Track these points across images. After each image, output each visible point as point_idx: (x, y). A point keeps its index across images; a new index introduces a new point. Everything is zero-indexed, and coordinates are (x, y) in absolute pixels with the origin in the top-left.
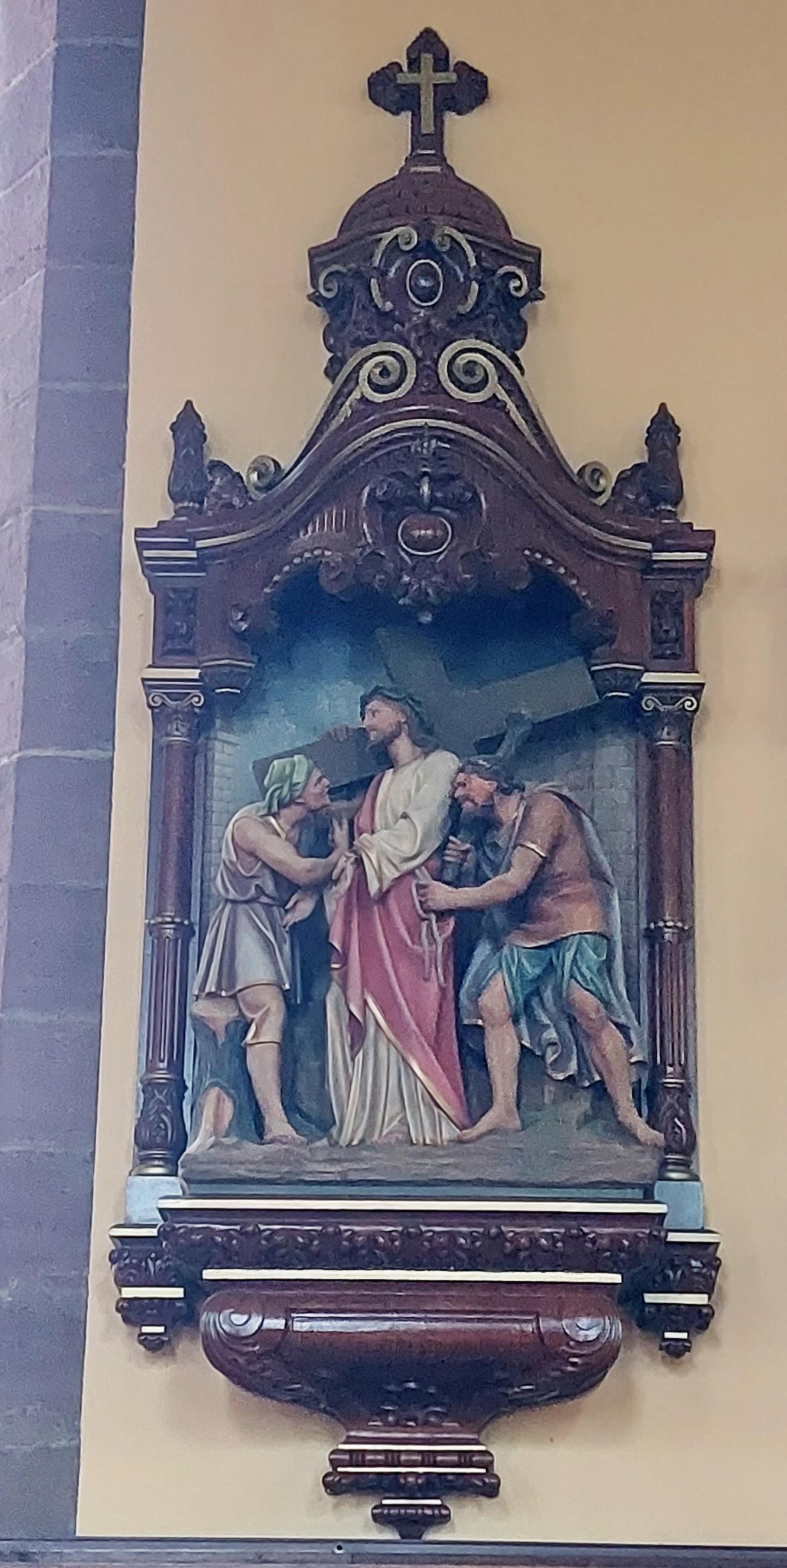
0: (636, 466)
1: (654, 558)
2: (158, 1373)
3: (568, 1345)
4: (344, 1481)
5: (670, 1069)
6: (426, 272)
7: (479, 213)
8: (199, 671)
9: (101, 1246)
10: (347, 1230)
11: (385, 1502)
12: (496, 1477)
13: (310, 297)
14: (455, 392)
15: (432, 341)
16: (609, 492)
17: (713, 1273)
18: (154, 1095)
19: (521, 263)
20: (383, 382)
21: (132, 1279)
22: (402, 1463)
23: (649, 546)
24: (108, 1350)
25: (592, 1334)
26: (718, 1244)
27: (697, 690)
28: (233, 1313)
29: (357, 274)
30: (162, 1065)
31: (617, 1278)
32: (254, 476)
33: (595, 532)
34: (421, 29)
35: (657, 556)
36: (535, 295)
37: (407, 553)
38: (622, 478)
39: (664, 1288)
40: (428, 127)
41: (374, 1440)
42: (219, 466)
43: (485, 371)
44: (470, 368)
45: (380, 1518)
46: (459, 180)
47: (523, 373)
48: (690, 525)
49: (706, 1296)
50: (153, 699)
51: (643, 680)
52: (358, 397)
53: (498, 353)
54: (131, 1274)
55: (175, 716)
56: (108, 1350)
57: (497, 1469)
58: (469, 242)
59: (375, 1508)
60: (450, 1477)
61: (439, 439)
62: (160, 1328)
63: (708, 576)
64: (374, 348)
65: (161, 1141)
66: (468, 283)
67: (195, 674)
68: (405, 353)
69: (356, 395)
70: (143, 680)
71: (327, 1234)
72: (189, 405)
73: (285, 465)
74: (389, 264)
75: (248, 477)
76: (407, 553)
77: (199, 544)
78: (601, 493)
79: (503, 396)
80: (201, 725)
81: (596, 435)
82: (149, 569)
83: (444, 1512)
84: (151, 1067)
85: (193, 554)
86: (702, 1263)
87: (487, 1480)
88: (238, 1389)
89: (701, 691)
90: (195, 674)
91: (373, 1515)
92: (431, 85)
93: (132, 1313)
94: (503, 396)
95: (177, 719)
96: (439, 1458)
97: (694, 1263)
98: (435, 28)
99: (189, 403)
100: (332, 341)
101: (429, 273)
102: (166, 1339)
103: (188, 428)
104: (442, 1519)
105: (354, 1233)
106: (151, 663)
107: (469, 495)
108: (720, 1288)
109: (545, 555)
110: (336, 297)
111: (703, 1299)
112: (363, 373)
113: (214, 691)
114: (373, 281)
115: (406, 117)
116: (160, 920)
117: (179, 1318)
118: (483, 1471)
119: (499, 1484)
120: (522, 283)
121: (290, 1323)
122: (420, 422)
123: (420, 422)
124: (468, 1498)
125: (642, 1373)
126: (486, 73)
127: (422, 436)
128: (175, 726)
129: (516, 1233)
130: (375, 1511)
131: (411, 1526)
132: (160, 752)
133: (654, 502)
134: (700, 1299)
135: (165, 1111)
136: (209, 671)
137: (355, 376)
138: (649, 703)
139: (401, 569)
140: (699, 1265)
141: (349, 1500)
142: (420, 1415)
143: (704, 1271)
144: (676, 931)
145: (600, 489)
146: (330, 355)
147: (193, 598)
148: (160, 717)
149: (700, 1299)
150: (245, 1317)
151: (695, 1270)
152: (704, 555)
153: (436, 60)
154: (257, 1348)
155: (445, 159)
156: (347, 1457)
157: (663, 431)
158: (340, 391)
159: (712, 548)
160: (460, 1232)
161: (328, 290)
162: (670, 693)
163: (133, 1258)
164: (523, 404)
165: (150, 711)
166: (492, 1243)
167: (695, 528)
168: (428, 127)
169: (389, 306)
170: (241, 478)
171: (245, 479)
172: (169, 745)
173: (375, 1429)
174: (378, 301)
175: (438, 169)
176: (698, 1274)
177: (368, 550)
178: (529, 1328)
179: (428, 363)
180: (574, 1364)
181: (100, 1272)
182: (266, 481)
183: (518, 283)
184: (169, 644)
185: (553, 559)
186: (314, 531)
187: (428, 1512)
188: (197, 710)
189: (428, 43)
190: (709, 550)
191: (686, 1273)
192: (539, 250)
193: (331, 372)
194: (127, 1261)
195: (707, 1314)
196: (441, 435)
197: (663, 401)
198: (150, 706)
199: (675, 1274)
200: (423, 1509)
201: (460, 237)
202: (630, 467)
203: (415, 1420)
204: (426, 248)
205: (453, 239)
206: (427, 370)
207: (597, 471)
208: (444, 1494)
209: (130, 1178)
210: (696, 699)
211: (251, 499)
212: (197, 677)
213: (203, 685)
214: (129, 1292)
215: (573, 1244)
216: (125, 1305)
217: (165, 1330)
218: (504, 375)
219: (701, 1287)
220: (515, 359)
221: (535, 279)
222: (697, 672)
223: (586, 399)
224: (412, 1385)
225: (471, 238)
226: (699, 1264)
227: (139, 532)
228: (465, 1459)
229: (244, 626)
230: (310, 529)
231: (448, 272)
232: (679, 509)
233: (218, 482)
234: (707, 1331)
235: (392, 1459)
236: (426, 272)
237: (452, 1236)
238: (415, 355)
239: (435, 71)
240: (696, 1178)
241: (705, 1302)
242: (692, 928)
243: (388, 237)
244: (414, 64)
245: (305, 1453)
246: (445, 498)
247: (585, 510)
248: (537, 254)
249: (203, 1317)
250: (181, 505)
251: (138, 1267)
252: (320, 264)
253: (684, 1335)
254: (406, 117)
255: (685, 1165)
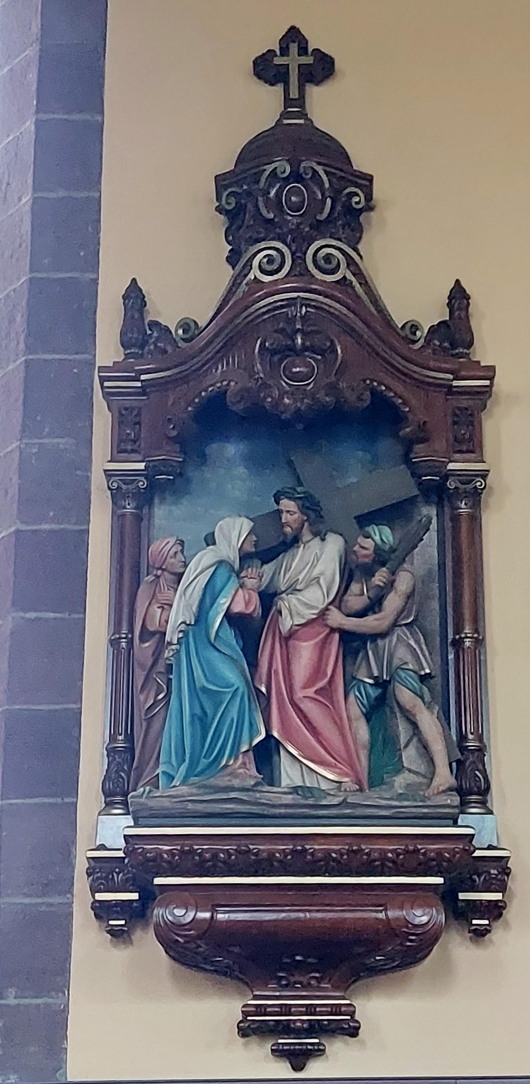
0: (440, 322)
1: (454, 385)
2: (121, 955)
3: (407, 927)
4: (252, 1026)
5: (471, 737)
6: (293, 191)
7: (332, 152)
8: (144, 464)
9: (81, 865)
10: (310, 849)
11: (280, 1041)
12: (358, 1022)
13: (217, 209)
14: (319, 275)
15: (298, 243)
16: (422, 340)
17: (506, 878)
18: (115, 759)
19: (357, 185)
20: (269, 268)
21: (102, 887)
22: (344, 1013)
23: (451, 377)
24: (87, 938)
25: (425, 919)
26: (509, 857)
27: (484, 475)
28: (174, 908)
29: (249, 193)
30: (120, 738)
31: (440, 880)
32: (180, 332)
33: (415, 368)
34: (289, 27)
35: (455, 383)
36: (369, 208)
37: (286, 383)
38: (432, 330)
39: (470, 890)
40: (294, 94)
41: (272, 998)
42: (155, 324)
43: (338, 260)
44: (328, 258)
45: (279, 1052)
46: (317, 129)
47: (361, 257)
48: (479, 362)
49: (501, 894)
50: (112, 484)
51: (448, 468)
52: (253, 278)
53: (344, 247)
54: (101, 884)
55: (127, 495)
56: (87, 938)
57: (357, 1017)
58: (325, 171)
59: (272, 1046)
60: (326, 1022)
61: (307, 306)
62: (122, 922)
63: (490, 396)
64: (263, 245)
65: (116, 794)
66: (324, 199)
67: (142, 466)
68: (285, 249)
69: (251, 276)
70: (105, 471)
71: (353, 851)
72: (134, 281)
73: (202, 324)
74: (271, 186)
75: (176, 331)
76: (286, 383)
77: (143, 377)
78: (417, 341)
79: (350, 276)
80: (146, 498)
81: (413, 301)
82: (107, 395)
83: (321, 1047)
84: (113, 738)
85: (139, 384)
86: (498, 871)
87: (351, 1024)
88: (177, 965)
89: (487, 475)
90: (142, 466)
91: (272, 1050)
92: (295, 65)
93: (102, 911)
94: (350, 276)
95: (128, 497)
96: (269, 1010)
97: (492, 871)
98: (297, 26)
99: (134, 280)
100: (231, 238)
101: (299, 193)
102: (126, 929)
103: (134, 297)
104: (318, 1052)
105: (259, 850)
106: (109, 459)
107: (328, 344)
108: (510, 888)
109: (380, 384)
110: (234, 208)
111: (499, 896)
112: (256, 262)
113: (154, 477)
114: (260, 199)
115: (279, 88)
116: (118, 636)
117: (137, 914)
118: (349, 1017)
119: (359, 1028)
120: (360, 199)
121: (215, 914)
122: (294, 295)
123: (294, 295)
124: (337, 1040)
125: (457, 947)
126: (333, 56)
127: (295, 305)
128: (127, 502)
129: (315, 850)
130: (273, 1048)
131: (298, 1058)
132: (118, 519)
133: (454, 346)
134: (497, 896)
135: (123, 771)
136: (151, 464)
137: (249, 264)
138: (451, 484)
139: (283, 394)
140: (497, 872)
141: (254, 1039)
142: (304, 980)
143: (499, 876)
144: (474, 640)
145: (416, 339)
146: (230, 247)
147: (139, 414)
148: (117, 496)
149: (497, 896)
150: (184, 911)
151: (493, 876)
152: (487, 383)
153: (300, 48)
154: (192, 932)
155: (306, 115)
156: (304, 1009)
157: (458, 297)
158: (239, 274)
159: (493, 377)
160: (331, 849)
161: (229, 204)
162: (467, 478)
163: (104, 872)
164: (364, 283)
165: (109, 492)
166: (356, 858)
167: (482, 364)
168: (294, 94)
169: (271, 216)
170: (171, 332)
171: (173, 332)
172: (124, 515)
173: (274, 990)
174: (264, 212)
175: (302, 121)
176: (494, 878)
177: (260, 382)
178: (382, 916)
179: (299, 254)
180: (411, 941)
181: (81, 883)
182: (190, 334)
183: (357, 199)
184: (120, 449)
185: (385, 386)
186: (223, 367)
187: (309, 1047)
188: (142, 491)
189: (293, 36)
190: (491, 379)
191: (487, 878)
192: (372, 176)
193: (233, 259)
194: (99, 875)
195: (502, 907)
196: (306, 303)
197: (457, 278)
198: (109, 488)
199: (479, 879)
200: (283, 1047)
201: (320, 169)
202: (436, 323)
203: (300, 983)
204: (296, 176)
205: (315, 172)
206: (299, 258)
207: (415, 327)
208: (320, 1035)
209: (100, 817)
210: (485, 481)
211: (179, 347)
212: (143, 468)
213: (149, 474)
214: (100, 896)
215: (411, 858)
216: (97, 905)
217: (126, 922)
218: (351, 262)
219: (497, 888)
220: (356, 250)
221: (369, 197)
222: (484, 462)
223: (406, 276)
224: (298, 958)
225: (328, 169)
226: (496, 872)
227: (99, 367)
228: (336, 1010)
229: (175, 433)
230: (220, 367)
231: (312, 194)
232: (471, 350)
233: (155, 334)
234: (502, 919)
235: (286, 1010)
236: (293, 191)
237: (328, 852)
238: (290, 250)
239: (299, 55)
240: (491, 813)
241: (501, 898)
242: (483, 639)
243: (272, 166)
244: (284, 51)
245: (224, 1008)
246: (312, 346)
247: (405, 352)
248: (370, 179)
249: (155, 911)
250: (129, 351)
251: (106, 879)
252: (222, 186)
253: (486, 922)
254: (279, 88)
255: (483, 803)
